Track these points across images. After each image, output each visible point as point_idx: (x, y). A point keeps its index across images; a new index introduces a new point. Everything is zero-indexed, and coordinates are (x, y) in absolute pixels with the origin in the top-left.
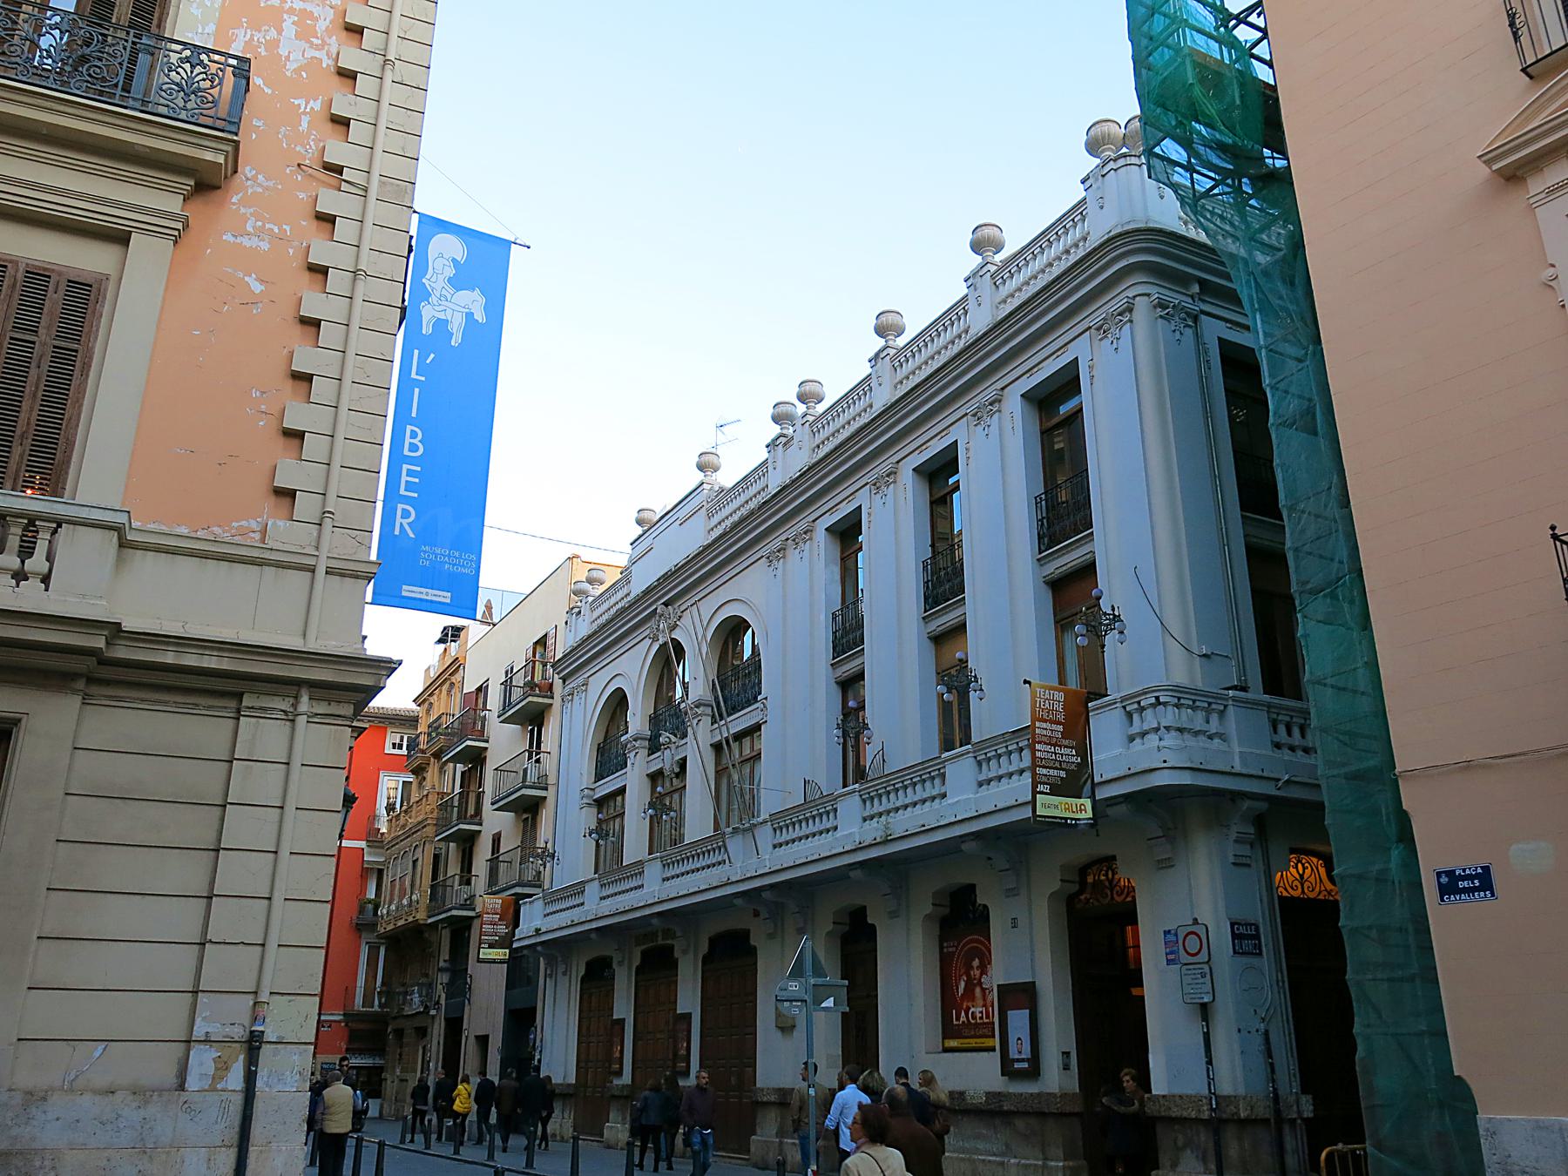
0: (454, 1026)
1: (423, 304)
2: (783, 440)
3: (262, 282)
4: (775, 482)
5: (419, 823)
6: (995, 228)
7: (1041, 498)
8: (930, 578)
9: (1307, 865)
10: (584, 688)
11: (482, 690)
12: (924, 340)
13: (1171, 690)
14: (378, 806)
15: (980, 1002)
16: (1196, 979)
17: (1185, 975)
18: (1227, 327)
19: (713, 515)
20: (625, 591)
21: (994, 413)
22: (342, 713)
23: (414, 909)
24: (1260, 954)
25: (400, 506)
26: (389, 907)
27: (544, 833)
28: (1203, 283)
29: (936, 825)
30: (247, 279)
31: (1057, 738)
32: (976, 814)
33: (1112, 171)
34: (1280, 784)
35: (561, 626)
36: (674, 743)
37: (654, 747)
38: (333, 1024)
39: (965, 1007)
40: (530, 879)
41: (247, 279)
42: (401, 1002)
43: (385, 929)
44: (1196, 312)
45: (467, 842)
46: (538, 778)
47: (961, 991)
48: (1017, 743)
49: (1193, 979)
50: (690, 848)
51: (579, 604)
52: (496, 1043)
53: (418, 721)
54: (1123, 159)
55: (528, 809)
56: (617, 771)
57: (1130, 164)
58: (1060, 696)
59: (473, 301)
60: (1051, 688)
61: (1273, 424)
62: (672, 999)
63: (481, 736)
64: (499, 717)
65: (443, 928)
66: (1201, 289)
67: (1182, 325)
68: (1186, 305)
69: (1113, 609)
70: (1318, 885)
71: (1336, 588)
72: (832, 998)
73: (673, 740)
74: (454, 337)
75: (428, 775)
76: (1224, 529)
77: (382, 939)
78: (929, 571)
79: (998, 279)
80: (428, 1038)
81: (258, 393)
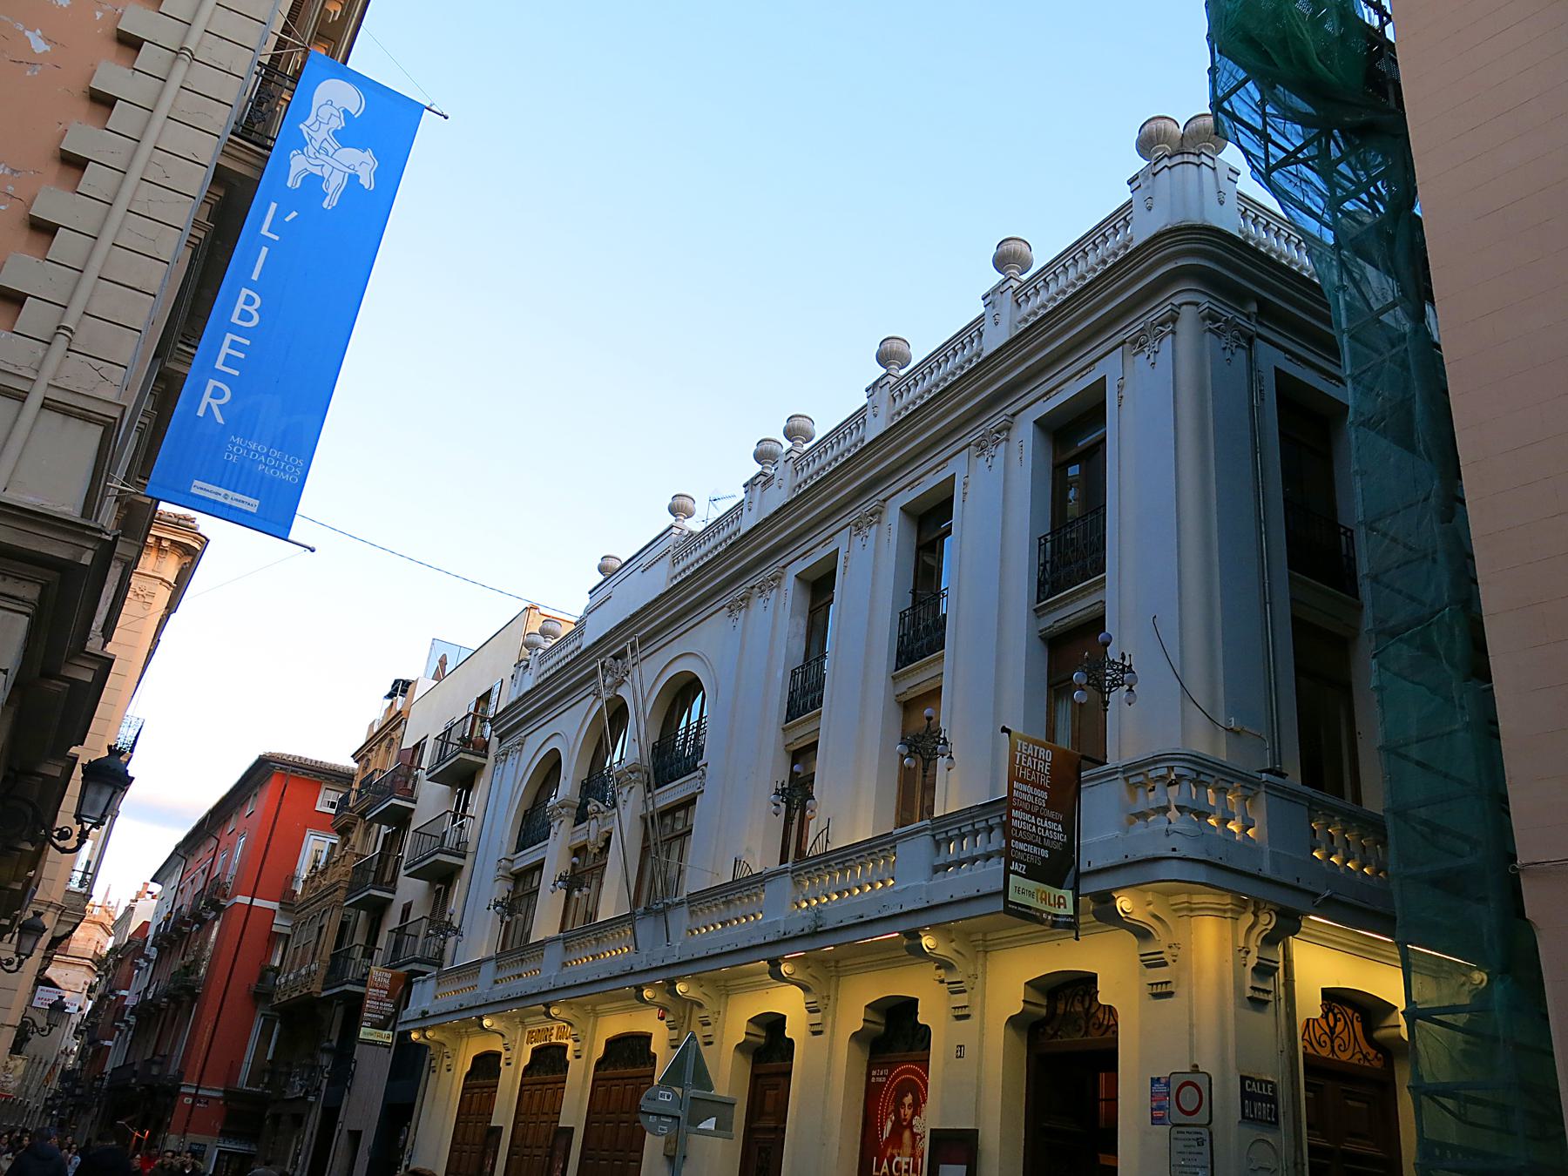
0: (330, 1116)
1: (295, 152)
2: (763, 479)
3: (48, 41)
4: (747, 523)
5: (333, 885)
6: (1023, 244)
7: (1046, 540)
8: (906, 632)
9: (1339, 1016)
10: (519, 748)
11: (419, 747)
12: (930, 367)
13: (1189, 761)
14: (298, 866)
15: (908, 1150)
16: (1189, 1146)
17: (1176, 1139)
18: (1286, 358)
19: (679, 562)
20: (577, 643)
21: (1001, 442)
22: (20, 595)
23: (310, 979)
24: (1277, 1123)
25: (212, 383)
26: (287, 976)
27: (455, 903)
28: (1263, 304)
29: (876, 916)
30: (27, 33)
31: (1040, 807)
32: (927, 905)
33: (1166, 169)
34: (1319, 900)
35: (508, 680)
36: (603, 813)
37: (581, 816)
38: (210, 1100)
39: (888, 1154)
40: (430, 956)
41: (27, 33)
42: (281, 1084)
43: (279, 999)
44: (1252, 333)
45: (378, 909)
46: (457, 845)
47: (886, 1134)
48: (987, 820)
49: (1185, 1146)
50: (595, 930)
51: (528, 657)
52: (367, 1140)
53: (353, 780)
54: (1180, 156)
55: (442, 878)
56: (540, 842)
57: (1187, 163)
58: (1047, 755)
59: (363, 163)
60: (1036, 743)
61: (1352, 423)
62: (557, 1108)
63: (410, 796)
64: (427, 774)
65: (338, 1005)
66: (1258, 309)
67: (1235, 344)
68: (1241, 322)
69: (1123, 658)
70: (1352, 1044)
71: (1429, 625)
72: (714, 1119)
73: (602, 810)
74: (328, 198)
75: (353, 837)
76: (1267, 585)
77: (275, 1011)
78: (906, 626)
79: (1021, 295)
80: (302, 1128)
81: (7, 169)
